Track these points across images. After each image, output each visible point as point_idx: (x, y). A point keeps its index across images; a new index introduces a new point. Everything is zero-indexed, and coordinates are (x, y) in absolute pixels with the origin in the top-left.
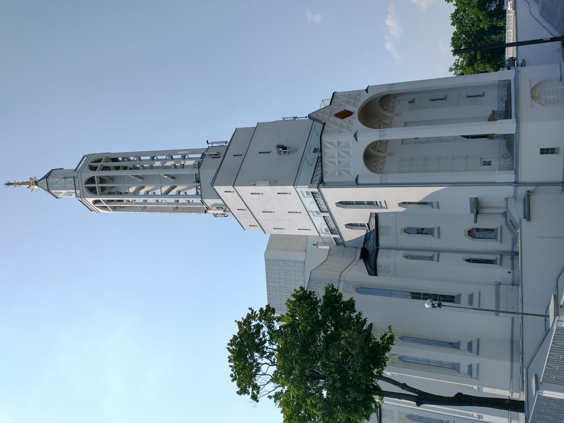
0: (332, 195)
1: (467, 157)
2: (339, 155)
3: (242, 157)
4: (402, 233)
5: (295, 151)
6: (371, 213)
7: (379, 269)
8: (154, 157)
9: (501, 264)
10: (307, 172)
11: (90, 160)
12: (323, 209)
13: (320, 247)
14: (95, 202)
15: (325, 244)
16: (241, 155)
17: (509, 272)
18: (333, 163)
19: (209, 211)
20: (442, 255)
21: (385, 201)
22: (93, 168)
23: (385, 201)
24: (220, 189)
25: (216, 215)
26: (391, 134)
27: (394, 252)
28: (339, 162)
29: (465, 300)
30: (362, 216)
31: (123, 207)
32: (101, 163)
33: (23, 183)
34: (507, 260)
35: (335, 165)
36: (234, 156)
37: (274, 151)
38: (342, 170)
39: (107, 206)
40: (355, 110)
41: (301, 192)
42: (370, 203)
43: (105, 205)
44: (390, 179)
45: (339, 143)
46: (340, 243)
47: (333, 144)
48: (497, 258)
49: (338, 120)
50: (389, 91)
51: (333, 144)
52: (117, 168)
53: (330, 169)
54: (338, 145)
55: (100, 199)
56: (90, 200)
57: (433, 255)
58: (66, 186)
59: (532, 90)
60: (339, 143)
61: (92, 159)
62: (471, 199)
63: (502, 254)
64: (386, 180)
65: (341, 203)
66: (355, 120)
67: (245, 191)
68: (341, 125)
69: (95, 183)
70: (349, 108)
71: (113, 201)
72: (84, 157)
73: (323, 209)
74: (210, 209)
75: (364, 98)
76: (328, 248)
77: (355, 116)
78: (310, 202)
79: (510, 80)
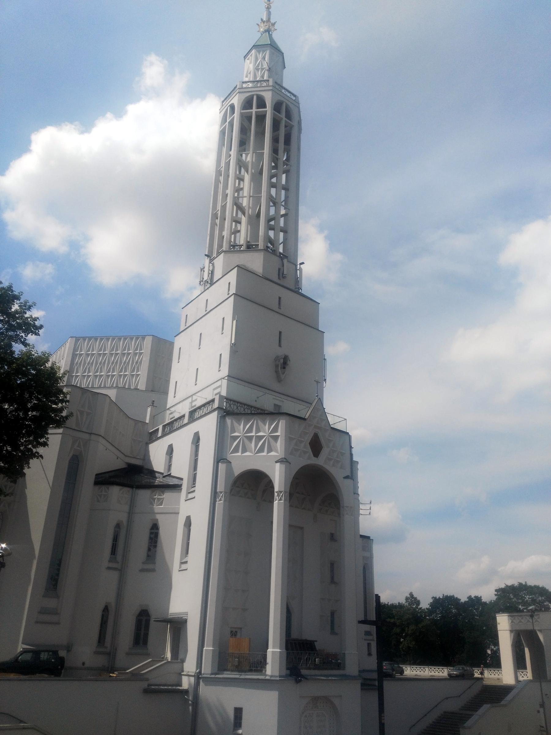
0: (208, 426)
3: (278, 310)
5: (279, 380)
6: (182, 479)
7: (104, 488)
9: (96, 653)
10: (247, 395)
12: (194, 415)
13: (149, 409)
14: (232, 107)
15: (153, 417)
17: (83, 664)
18: (250, 430)
19: (207, 261)
20: (115, 575)
22: (277, 107)
24: (232, 277)
25: (202, 270)
26: (278, 507)
27: (126, 508)
28: (250, 438)
29: (51, 603)
30: (180, 468)
32: (284, 119)
33: (269, 14)
34: (101, 661)
35: (246, 433)
37: (281, 352)
39: (227, 123)
40: (320, 461)
41: (220, 386)
43: (228, 121)
44: (220, 504)
45: (276, 438)
46: (153, 437)
47: (275, 429)
49: (308, 438)
50: (343, 507)
52: (275, 140)
53: (240, 429)
55: (235, 115)
56: (236, 101)
57: (118, 563)
58: (258, 70)
59: (327, 700)
60: (276, 438)
62: (187, 614)
63: (111, 655)
64: (220, 500)
65: (198, 439)
66: (308, 459)
68: (301, 442)
70: (324, 453)
72: (295, 96)
73: (194, 415)
74: (210, 263)
75: (337, 474)
76: (147, 421)
77: (313, 461)
78: (207, 395)
79: (344, 668)
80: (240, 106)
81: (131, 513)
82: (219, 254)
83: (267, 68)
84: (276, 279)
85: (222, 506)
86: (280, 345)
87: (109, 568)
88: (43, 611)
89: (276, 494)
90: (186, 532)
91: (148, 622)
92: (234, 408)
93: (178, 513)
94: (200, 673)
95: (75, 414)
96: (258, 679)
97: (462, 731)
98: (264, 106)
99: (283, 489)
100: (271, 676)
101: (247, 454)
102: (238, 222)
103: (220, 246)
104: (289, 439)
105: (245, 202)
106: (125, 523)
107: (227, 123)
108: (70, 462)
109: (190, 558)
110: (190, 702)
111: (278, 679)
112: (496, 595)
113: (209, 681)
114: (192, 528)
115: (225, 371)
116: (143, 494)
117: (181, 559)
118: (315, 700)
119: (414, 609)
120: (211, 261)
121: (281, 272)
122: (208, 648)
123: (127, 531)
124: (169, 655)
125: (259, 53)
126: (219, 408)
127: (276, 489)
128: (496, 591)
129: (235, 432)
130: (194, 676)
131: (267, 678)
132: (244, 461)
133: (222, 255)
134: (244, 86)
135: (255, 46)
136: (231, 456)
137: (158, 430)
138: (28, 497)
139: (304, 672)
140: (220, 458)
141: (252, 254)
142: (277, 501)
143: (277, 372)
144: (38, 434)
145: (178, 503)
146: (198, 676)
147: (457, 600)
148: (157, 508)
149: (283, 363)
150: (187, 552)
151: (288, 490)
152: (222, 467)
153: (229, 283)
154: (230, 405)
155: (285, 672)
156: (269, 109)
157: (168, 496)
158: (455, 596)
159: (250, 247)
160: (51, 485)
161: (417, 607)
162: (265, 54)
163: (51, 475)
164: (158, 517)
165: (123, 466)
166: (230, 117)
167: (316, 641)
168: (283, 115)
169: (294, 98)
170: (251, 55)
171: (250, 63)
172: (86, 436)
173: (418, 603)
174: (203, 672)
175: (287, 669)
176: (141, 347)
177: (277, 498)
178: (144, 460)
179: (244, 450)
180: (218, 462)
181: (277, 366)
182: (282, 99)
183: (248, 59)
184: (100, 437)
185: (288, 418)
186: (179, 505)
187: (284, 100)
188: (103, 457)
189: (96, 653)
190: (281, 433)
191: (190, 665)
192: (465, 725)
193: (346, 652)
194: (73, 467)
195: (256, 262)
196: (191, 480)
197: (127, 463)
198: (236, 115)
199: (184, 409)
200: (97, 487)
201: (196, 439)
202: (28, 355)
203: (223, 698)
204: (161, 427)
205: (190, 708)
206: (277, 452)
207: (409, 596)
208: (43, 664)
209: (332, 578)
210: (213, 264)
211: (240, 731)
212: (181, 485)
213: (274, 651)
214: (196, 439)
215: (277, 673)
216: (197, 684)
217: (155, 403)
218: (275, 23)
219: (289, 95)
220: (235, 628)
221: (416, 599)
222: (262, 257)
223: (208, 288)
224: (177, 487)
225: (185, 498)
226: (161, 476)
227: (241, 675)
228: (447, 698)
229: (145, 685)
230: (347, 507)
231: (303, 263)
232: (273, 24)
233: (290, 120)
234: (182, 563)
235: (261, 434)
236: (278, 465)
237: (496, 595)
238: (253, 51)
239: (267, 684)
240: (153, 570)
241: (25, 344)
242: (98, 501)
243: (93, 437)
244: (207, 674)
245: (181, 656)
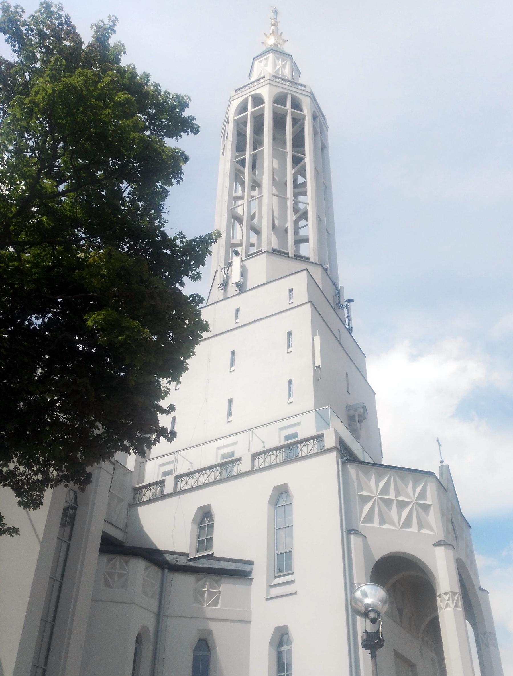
2: (402, 505)
4: (200, 631)
7: (118, 561)
14: (258, 100)
27: (154, 605)
28: (388, 503)
30: (239, 536)
36: (230, 401)
38: (413, 506)
45: (426, 508)
51: (423, 495)
60: (426, 508)
64: (447, 606)
93: (250, 622)
125: (278, 59)
129: (362, 490)
136: (362, 527)
138: (412, 553)
148: (209, 610)
157: (227, 588)
164: (213, 626)
200: (105, 558)
225: (265, 595)
231: (351, 301)
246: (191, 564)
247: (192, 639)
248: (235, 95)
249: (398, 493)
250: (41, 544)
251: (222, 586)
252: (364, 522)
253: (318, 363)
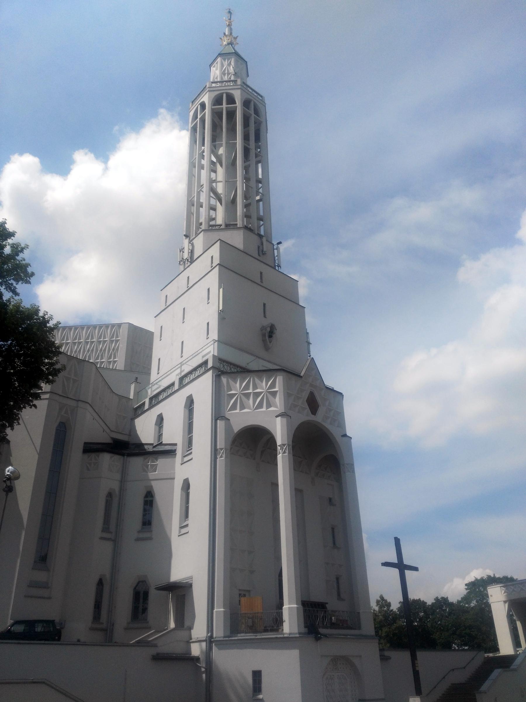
0: (203, 389)
1: (252, 572)
3: (260, 283)
5: (267, 348)
7: (93, 455)
8: (260, 182)
9: (92, 629)
11: (256, 102)
13: (133, 386)
15: (137, 393)
16: (262, 282)
18: (247, 387)
19: (186, 241)
20: (108, 546)
21: (192, 459)
22: (246, 103)
23: (192, 459)
24: (215, 251)
25: (182, 250)
26: (283, 462)
27: (118, 476)
28: (247, 396)
29: (41, 576)
30: (173, 434)
31: (196, 142)
32: (253, 115)
33: (231, 30)
37: (266, 322)
39: (198, 119)
40: (319, 418)
42: (189, 443)
43: (199, 117)
44: (221, 461)
45: (274, 394)
46: (139, 411)
47: (273, 385)
48: (102, 623)
49: (305, 395)
53: (237, 387)
54: (270, 392)
56: (206, 98)
57: (111, 533)
61: (260, 106)
64: (221, 457)
66: (306, 416)
67: (213, 280)
69: (227, 104)
71: (204, 128)
72: (262, 97)
74: (190, 243)
76: (131, 397)
77: (311, 418)
79: (359, 628)
80: (211, 103)
81: (123, 481)
82: (197, 235)
83: (234, 73)
84: (256, 256)
85: (224, 463)
86: (265, 316)
87: (102, 538)
88: (34, 585)
89: (279, 448)
90: (184, 496)
91: (146, 594)
92: (227, 368)
94: (211, 637)
95: (68, 369)
96: (277, 638)
97: (478, 696)
98: (234, 102)
99: (286, 443)
100: (290, 634)
101: (246, 410)
102: (214, 209)
103: (198, 228)
104: (288, 395)
105: (220, 188)
106: (117, 490)
107: (198, 119)
108: (57, 430)
109: (190, 521)
110: (203, 670)
111: (298, 635)
112: (466, 589)
113: (222, 644)
114: (191, 491)
115: (214, 335)
116: (136, 462)
117: (181, 522)
118: (336, 660)
119: (386, 611)
120: (190, 242)
121: (261, 248)
122: (219, 610)
123: (120, 499)
124: (172, 625)
125: (225, 60)
126: (213, 367)
127: (279, 442)
128: (466, 585)
129: (231, 390)
130: (205, 641)
131: (285, 636)
132: (243, 417)
133: (202, 234)
134: (214, 85)
135: (220, 55)
136: (228, 414)
137: (144, 404)
139: (322, 631)
140: (218, 415)
141: (231, 232)
142: (281, 455)
143: (264, 341)
144: (27, 397)
145: (173, 468)
146: (210, 641)
147: (424, 603)
148: (152, 475)
149: (269, 333)
150: (187, 516)
151: (291, 443)
152: (220, 424)
153: (212, 257)
154: (224, 366)
155: (304, 630)
156: (239, 104)
157: (161, 462)
158: (422, 600)
159: (229, 226)
160: (38, 451)
161: (388, 609)
162: (231, 62)
163: (38, 442)
164: (153, 483)
165: (109, 441)
166: (200, 114)
167: (327, 603)
168: (252, 112)
169: (261, 98)
170: (217, 63)
171: (217, 69)
172: (73, 403)
173: (389, 605)
174: (214, 636)
175: (305, 627)
176: (117, 334)
177: (281, 451)
178: (130, 435)
179: (242, 407)
180: (216, 420)
181: (264, 335)
182: (251, 98)
183: (214, 67)
184: (88, 405)
185: (284, 374)
186: (174, 470)
187: (252, 99)
188: (89, 427)
189: (92, 629)
190: (279, 389)
191: (199, 630)
192: (481, 689)
193: (361, 611)
194: (60, 435)
195: (237, 239)
196: (186, 444)
197: (112, 438)
198: (207, 111)
199: (174, 378)
201: (190, 403)
202: (18, 307)
203: (235, 663)
204: (147, 401)
205: (204, 675)
206: (276, 407)
207: (379, 599)
208: (41, 632)
209: (334, 543)
210: (192, 245)
211: (261, 697)
212: (175, 450)
213: (290, 609)
214: (190, 403)
215: (296, 630)
216: (209, 649)
217: (138, 379)
218: (185, 235)
219: (256, 95)
220: (244, 590)
221: (386, 601)
222: (242, 233)
223: (189, 266)
224: (170, 453)
226: (151, 447)
227: (256, 636)
228: (453, 670)
229: (153, 651)
230: (347, 464)
231: (280, 243)
232: (235, 38)
233: (258, 116)
234: (181, 528)
235: (258, 390)
236: (279, 419)
237: (466, 589)
238: (219, 59)
239: (287, 642)
240: (150, 539)
241: (14, 292)
242: (88, 469)
243: (81, 404)
244: (219, 637)
245: (187, 623)
246: (155, 449)
247: (143, 493)
248: (192, 105)
249: (255, 387)
250: (39, 454)
251: (159, 460)
252: (230, 410)
253: (221, 308)
